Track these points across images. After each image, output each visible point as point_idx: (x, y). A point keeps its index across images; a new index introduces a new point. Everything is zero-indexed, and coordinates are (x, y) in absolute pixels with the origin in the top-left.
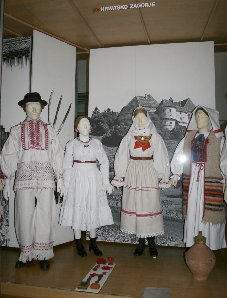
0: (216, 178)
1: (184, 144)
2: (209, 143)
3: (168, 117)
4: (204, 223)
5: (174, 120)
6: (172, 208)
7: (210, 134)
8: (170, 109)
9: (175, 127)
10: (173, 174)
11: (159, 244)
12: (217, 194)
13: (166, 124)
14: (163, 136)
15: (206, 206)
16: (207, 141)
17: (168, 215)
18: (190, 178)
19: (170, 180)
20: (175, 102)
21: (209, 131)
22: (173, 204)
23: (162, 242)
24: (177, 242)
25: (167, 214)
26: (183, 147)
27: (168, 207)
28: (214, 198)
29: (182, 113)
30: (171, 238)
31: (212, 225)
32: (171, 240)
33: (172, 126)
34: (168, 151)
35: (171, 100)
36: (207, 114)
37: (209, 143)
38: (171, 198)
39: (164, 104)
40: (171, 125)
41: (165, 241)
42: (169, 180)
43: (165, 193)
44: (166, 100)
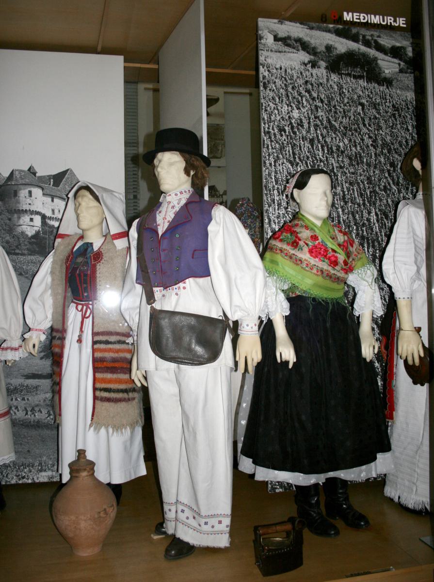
0: (118, 334)
1: (54, 262)
2: (101, 260)
3: (26, 207)
4: (95, 429)
5: (38, 213)
6: (37, 401)
7: (105, 240)
8: (29, 189)
9: (40, 229)
10: (30, 330)
11: (13, 482)
12: (122, 368)
13: (21, 222)
14: (15, 247)
15: (98, 393)
16: (98, 256)
17: (29, 416)
18: (63, 335)
19: (24, 343)
20: (41, 177)
21: (104, 236)
22: (39, 393)
23: (19, 475)
24: (53, 471)
25: (27, 414)
26: (49, 270)
27: (28, 399)
28: (115, 376)
29: (55, 200)
30: (39, 466)
31: (113, 432)
32: (38, 468)
33: (33, 226)
34: (19, 280)
35: (31, 171)
36: (97, 198)
37: (101, 261)
38: (35, 380)
39: (16, 180)
40: (31, 224)
41: (25, 472)
42: (23, 341)
43: (21, 370)
44: (20, 171)
